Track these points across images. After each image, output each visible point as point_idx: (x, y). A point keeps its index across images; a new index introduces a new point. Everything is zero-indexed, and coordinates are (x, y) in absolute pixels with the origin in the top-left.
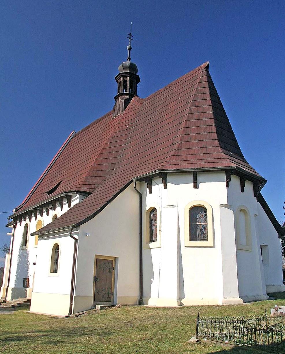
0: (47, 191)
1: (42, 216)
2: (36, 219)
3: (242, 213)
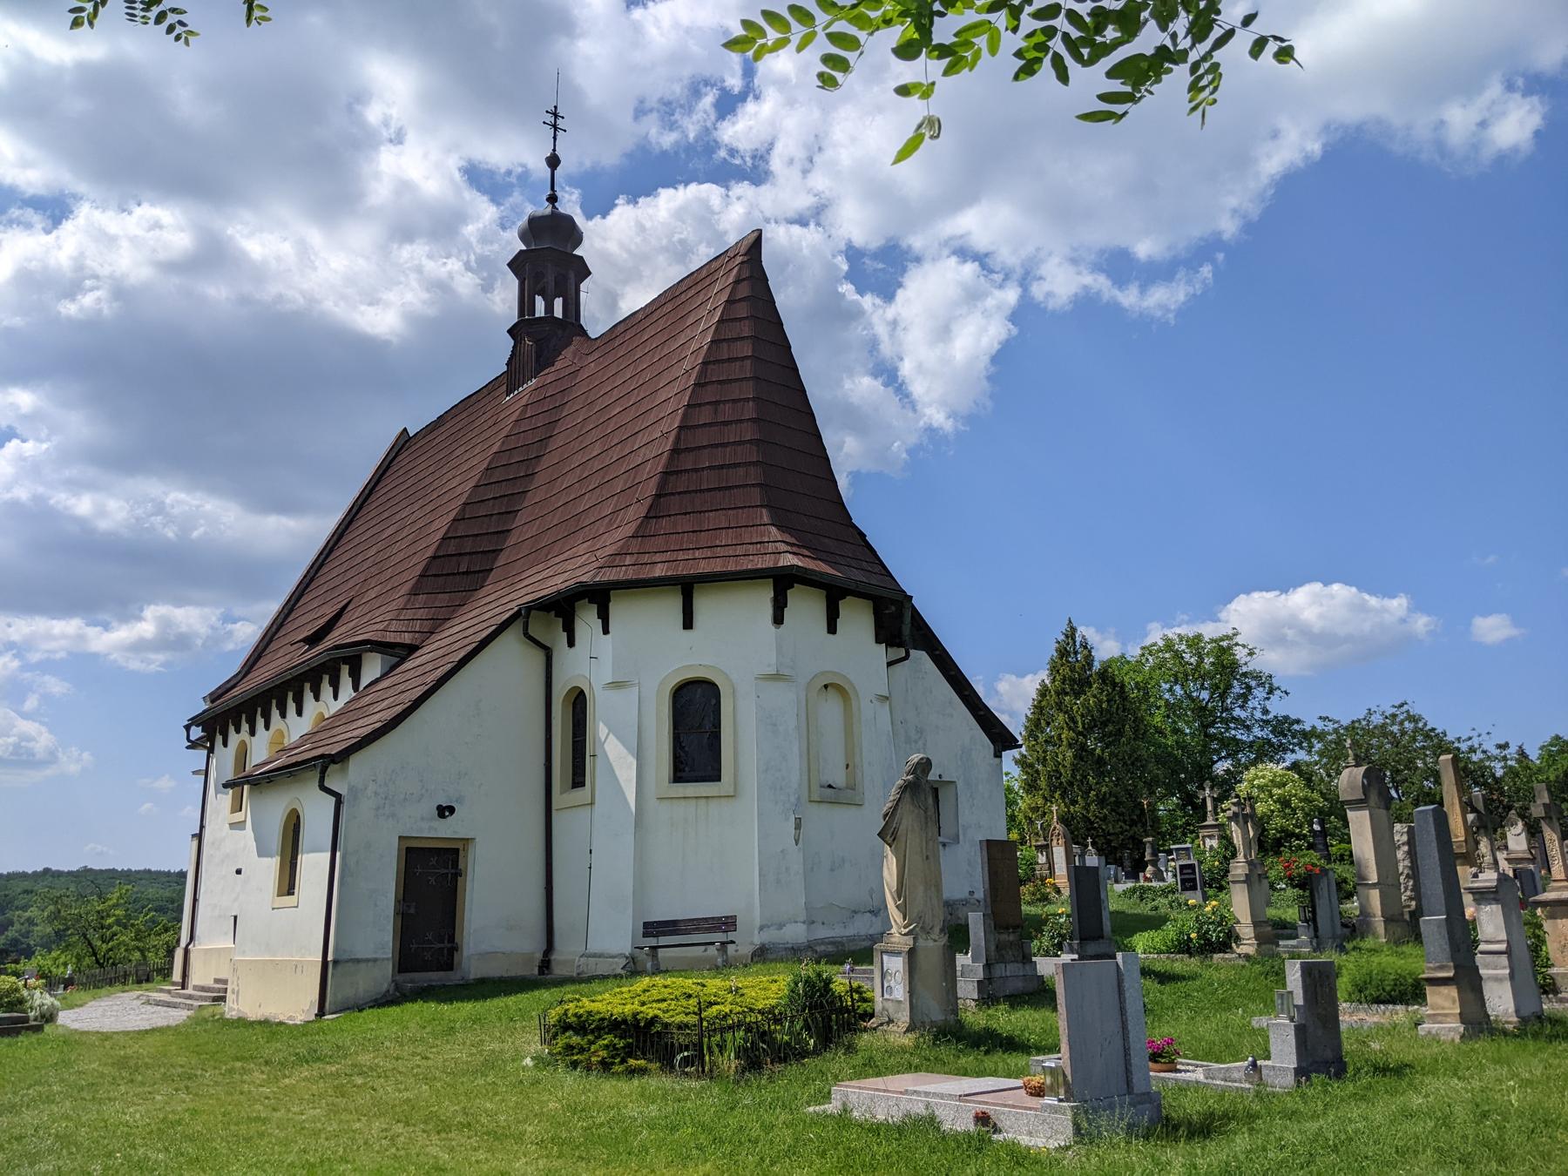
1: (283, 715)
2: (267, 727)
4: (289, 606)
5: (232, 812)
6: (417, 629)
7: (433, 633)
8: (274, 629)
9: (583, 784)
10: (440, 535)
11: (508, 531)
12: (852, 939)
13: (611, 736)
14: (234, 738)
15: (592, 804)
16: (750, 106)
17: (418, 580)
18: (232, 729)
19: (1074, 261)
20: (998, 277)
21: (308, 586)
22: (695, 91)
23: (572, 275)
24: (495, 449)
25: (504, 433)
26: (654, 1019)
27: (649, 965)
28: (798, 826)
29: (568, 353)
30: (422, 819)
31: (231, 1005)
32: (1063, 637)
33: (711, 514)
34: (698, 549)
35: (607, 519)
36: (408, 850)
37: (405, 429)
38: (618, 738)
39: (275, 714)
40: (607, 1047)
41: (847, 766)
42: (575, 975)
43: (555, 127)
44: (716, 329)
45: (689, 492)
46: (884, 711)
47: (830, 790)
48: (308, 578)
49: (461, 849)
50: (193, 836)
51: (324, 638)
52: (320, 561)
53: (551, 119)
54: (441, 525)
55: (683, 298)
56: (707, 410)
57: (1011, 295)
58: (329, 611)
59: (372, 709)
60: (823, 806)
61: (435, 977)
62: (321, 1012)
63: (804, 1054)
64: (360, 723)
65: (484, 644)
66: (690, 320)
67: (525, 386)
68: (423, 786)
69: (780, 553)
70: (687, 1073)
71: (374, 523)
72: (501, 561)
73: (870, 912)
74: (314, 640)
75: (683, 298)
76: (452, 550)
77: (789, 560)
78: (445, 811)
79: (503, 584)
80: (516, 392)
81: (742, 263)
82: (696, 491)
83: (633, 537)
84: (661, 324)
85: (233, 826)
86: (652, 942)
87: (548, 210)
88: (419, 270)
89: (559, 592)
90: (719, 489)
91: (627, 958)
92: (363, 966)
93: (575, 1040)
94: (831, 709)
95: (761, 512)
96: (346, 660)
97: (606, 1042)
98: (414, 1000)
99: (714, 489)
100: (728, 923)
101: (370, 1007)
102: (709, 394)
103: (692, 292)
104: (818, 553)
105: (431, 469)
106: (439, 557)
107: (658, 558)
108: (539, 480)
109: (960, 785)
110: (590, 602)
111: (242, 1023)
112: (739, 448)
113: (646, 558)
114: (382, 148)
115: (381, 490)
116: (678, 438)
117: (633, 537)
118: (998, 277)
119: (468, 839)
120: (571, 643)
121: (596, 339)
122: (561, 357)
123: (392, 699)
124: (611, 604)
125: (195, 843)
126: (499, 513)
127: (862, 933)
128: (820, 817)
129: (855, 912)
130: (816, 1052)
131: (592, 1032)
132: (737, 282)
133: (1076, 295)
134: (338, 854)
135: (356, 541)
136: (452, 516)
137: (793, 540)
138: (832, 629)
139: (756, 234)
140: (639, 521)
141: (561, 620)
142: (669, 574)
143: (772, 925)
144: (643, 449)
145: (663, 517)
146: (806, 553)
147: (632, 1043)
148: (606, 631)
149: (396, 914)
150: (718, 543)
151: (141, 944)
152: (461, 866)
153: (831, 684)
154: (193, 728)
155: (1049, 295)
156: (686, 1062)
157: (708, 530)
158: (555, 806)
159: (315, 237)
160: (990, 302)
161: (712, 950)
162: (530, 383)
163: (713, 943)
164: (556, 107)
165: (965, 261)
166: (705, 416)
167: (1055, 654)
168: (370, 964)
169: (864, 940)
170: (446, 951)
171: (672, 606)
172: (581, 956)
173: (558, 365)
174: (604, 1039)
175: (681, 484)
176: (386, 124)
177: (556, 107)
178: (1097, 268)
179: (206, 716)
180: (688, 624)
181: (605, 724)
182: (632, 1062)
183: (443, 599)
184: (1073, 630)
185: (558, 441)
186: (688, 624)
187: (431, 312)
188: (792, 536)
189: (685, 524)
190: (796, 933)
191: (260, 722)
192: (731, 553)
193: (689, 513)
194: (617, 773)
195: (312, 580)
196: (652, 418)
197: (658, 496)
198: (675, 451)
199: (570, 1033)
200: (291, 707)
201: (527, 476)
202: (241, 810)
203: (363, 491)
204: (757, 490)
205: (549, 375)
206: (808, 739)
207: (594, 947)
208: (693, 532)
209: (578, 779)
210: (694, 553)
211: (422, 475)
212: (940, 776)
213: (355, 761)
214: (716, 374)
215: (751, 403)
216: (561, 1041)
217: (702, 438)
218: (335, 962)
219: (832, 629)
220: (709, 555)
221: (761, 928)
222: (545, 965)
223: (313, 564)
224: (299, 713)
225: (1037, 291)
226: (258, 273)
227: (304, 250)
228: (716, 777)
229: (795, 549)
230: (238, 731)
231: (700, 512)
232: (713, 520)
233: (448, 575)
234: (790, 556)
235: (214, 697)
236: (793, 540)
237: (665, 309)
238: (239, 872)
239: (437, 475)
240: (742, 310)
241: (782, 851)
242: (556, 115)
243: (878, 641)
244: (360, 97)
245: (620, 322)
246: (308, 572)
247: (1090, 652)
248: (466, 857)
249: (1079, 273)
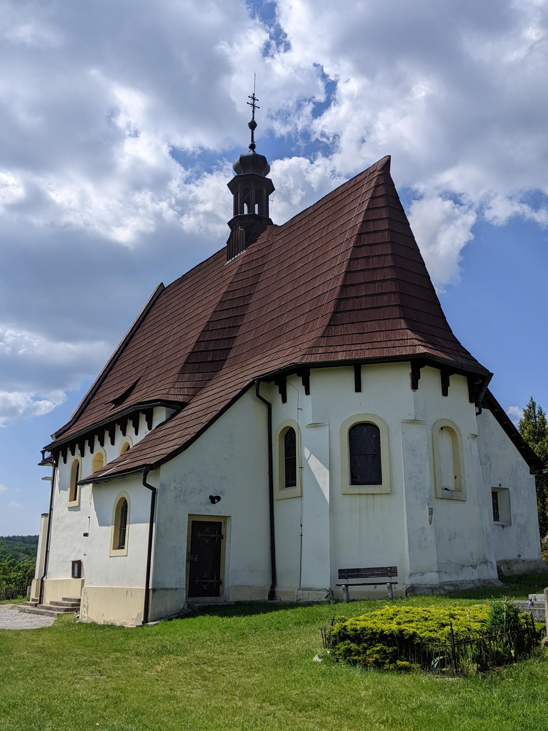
0: (111, 400)
1: (102, 445)
2: (92, 452)
3: (445, 434)
4: (98, 384)
5: (70, 501)
6: (186, 393)
7: (195, 396)
8: (90, 397)
9: (294, 485)
10: (194, 340)
11: (235, 337)
12: (462, 582)
13: (312, 456)
14: (71, 459)
15: (301, 496)
16: (333, 109)
17: (184, 365)
18: (69, 453)
19: (510, 198)
20: (466, 207)
21: (109, 372)
22: (299, 106)
23: (265, 191)
24: (224, 290)
25: (229, 281)
26: (414, 635)
27: (345, 596)
28: (431, 513)
29: (265, 234)
30: (201, 504)
31: (83, 614)
32: (527, 408)
33: (369, 323)
34: (363, 344)
35: (301, 328)
36: (193, 522)
37: (162, 283)
38: (315, 456)
39: (97, 443)
40: (378, 652)
41: (455, 477)
42: (295, 601)
43: (253, 105)
44: (365, 214)
45: (354, 310)
46: (474, 444)
47: (446, 491)
48: (109, 367)
49: (223, 522)
50: (44, 515)
51: (123, 402)
52: (116, 358)
53: (251, 101)
54: (194, 335)
55: (339, 198)
56: (362, 261)
57: (471, 219)
58: (126, 386)
59: (167, 438)
60: (444, 501)
61: (208, 600)
62: (146, 621)
63: (512, 660)
64: (162, 446)
65: (235, 400)
66: (347, 210)
67: (239, 255)
68: (201, 484)
69: (415, 346)
70: (443, 673)
71: (148, 335)
72: (232, 354)
73: (471, 566)
74: (118, 402)
75: (339, 198)
76: (202, 348)
77: (421, 350)
78: (214, 499)
79: (235, 367)
80: (233, 258)
81: (379, 175)
82: (358, 310)
83: (321, 337)
84: (325, 215)
85: (70, 509)
86: (344, 581)
87: (251, 153)
88: (145, 207)
89: (280, 369)
90: (373, 308)
91: (328, 591)
92: (169, 592)
93: (353, 646)
94: (445, 441)
95: (400, 321)
96: (144, 412)
97: (378, 648)
98: (203, 614)
99: (370, 308)
100: (392, 571)
101: (177, 618)
102: (363, 252)
103: (346, 194)
104: (436, 346)
105: (183, 304)
106: (195, 352)
107: (338, 349)
108: (252, 308)
109: (511, 490)
110: (298, 375)
111: (93, 626)
112: (384, 284)
113: (331, 349)
114: (126, 141)
115: (149, 318)
116: (345, 279)
117: (321, 337)
118: (466, 207)
119: (226, 517)
120: (284, 400)
121: (282, 226)
122: (260, 237)
123: (180, 433)
124: (310, 377)
126: (229, 327)
127: (468, 579)
128: (440, 506)
129: (463, 566)
130: (515, 660)
131: (366, 641)
132: (377, 186)
133: (510, 217)
134: (154, 524)
135: (138, 346)
136: (201, 329)
137: (421, 338)
138: (445, 393)
139: (387, 158)
140: (324, 327)
141: (132, 421)
142: (347, 358)
143: (417, 573)
144: (322, 286)
145: (339, 325)
146: (431, 346)
147: (397, 650)
148: (307, 393)
149: (187, 561)
150: (375, 340)
151: (6, 577)
152: (223, 533)
153: (444, 427)
154: (46, 452)
155: (495, 217)
156: (442, 664)
157: (368, 333)
158: (275, 497)
159: (89, 188)
160: (459, 222)
161: (384, 588)
162: (242, 253)
163: (386, 583)
164: (254, 94)
165: (445, 200)
166: (361, 265)
167: (523, 418)
168: (174, 591)
169: (469, 583)
170: (215, 584)
171: (349, 378)
172: (299, 589)
173: (259, 242)
174: (376, 647)
175: (349, 305)
176: (129, 125)
177: (254, 94)
178: (522, 202)
179: (55, 446)
180: (358, 389)
181: (308, 448)
182: (399, 662)
183: (198, 376)
184: (534, 404)
185: (262, 285)
186: (358, 389)
187: (152, 229)
188: (420, 336)
189: (353, 329)
190: (432, 578)
191: (87, 449)
192: (384, 346)
193: (355, 323)
194: (317, 478)
195: (111, 369)
196: (326, 268)
197: (335, 313)
198: (344, 286)
199: (348, 641)
200: (107, 439)
201: (244, 305)
202: (75, 499)
203: (139, 318)
204: (397, 308)
205: (254, 248)
206: (434, 461)
207: (305, 583)
208: (358, 333)
210: (361, 346)
211: (176, 308)
212: (500, 485)
213: (164, 468)
214: (367, 240)
215: (389, 257)
216: (342, 647)
217: (360, 278)
218: (154, 590)
219: (445, 393)
220: (370, 347)
221: (411, 575)
222: (272, 594)
223: (112, 359)
224: (113, 443)
225: (488, 215)
226: (60, 210)
227: (83, 197)
228: (378, 481)
229: (423, 344)
230: (73, 454)
231: (362, 322)
232: (369, 326)
233: (201, 362)
234: (422, 347)
235: (58, 435)
236: (421, 338)
237: (327, 206)
238: (86, 535)
239: (187, 307)
240: (381, 202)
241: (422, 528)
242: (254, 99)
243: (471, 401)
244: (113, 112)
245: (297, 215)
246: (109, 364)
247: (544, 416)
248: (225, 527)
249: (513, 205)
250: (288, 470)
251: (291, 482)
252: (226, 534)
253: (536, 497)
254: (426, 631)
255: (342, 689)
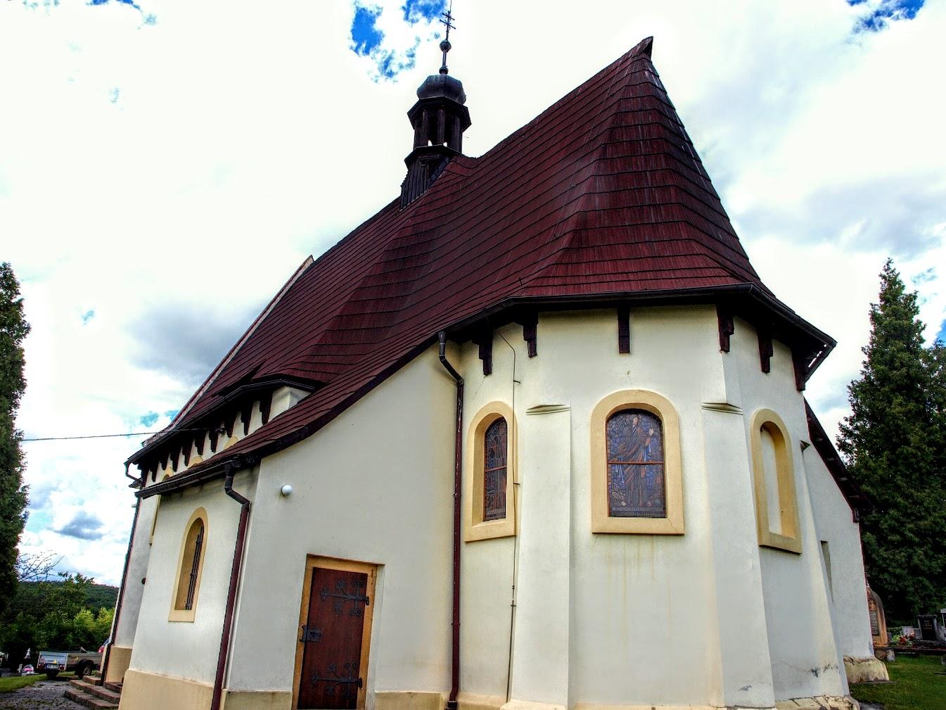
43: (448, 25)
120: (488, 371)
125: (135, 509)
139: (650, 40)
154: (132, 465)
177: (449, 12)
186: (624, 347)
209: (494, 504)
248: (374, 584)
250: (489, 490)
251: (494, 512)
252: (374, 595)
253: (463, 87)
254: (605, 149)
255: (619, 457)
